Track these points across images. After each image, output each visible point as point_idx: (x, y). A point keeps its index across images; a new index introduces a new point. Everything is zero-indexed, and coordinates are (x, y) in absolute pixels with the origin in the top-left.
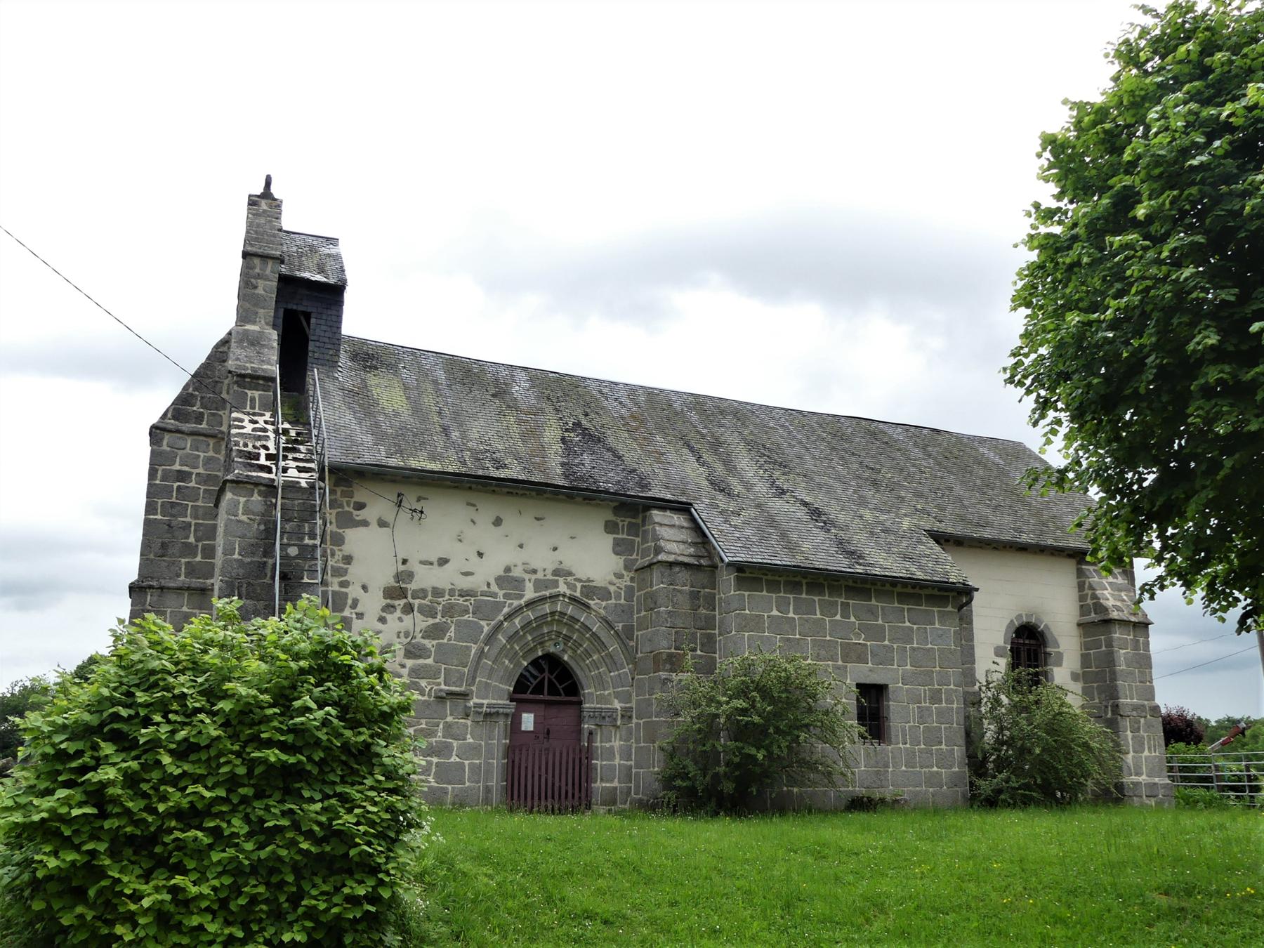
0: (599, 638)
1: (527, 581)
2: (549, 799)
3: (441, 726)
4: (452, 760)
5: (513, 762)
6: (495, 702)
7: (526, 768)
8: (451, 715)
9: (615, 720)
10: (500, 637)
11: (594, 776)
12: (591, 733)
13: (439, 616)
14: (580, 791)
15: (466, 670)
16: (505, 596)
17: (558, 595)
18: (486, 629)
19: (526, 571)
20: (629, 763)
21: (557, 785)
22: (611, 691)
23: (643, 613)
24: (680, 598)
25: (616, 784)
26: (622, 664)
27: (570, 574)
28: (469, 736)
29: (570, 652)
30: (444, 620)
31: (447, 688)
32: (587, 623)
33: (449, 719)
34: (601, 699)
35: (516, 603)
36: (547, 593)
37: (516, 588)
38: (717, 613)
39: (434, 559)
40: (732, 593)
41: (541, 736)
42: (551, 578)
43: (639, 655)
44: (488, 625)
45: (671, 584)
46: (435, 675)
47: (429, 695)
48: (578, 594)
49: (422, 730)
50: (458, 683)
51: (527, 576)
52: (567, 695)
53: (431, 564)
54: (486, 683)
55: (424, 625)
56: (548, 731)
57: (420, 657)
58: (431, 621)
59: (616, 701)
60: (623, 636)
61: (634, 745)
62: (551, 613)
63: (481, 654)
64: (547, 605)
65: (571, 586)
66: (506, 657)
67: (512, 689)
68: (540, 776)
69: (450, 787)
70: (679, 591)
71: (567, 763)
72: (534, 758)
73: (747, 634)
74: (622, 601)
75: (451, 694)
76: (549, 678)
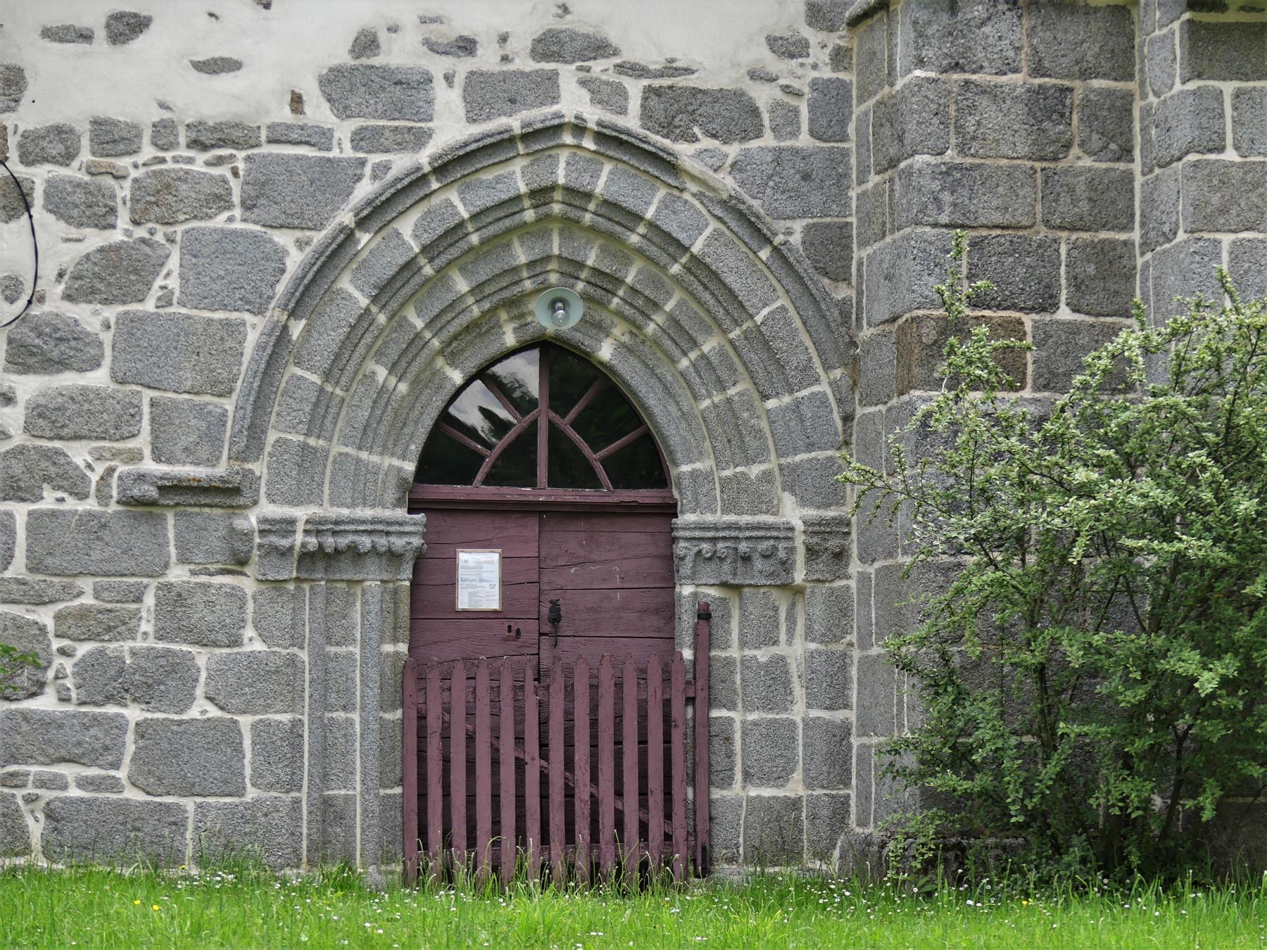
0: (715, 276)
1: (439, 86)
2: (533, 841)
3: (150, 600)
4: (194, 713)
5: (422, 718)
6: (345, 512)
7: (471, 738)
8: (183, 560)
9: (787, 565)
10: (345, 283)
11: (719, 760)
12: (704, 615)
13: (123, 219)
14: (668, 816)
15: (229, 405)
16: (359, 139)
17: (557, 129)
18: (295, 260)
19: (433, 47)
20: (839, 715)
21: (583, 793)
22: (772, 464)
23: (874, 179)
24: (990, 115)
25: (795, 788)
26: (807, 368)
27: (600, 48)
28: (249, 632)
29: (620, 331)
30: (141, 232)
31: (164, 468)
32: (671, 226)
33: (178, 574)
34: (737, 492)
35: (401, 163)
36: (515, 123)
37: (398, 110)
38: (1137, 167)
39: (95, 20)
40: (1178, 86)
41: (529, 629)
42: (530, 65)
43: (866, 333)
44: (301, 245)
45: (957, 67)
46: (123, 425)
47: (103, 497)
48: (631, 121)
49: (83, 614)
50: (204, 452)
51: (438, 66)
52: (617, 483)
53: (85, 36)
54: (304, 447)
55: (69, 255)
56: (555, 605)
57: (62, 365)
58: (94, 239)
59: (788, 500)
60: (805, 267)
61: (856, 654)
62: (533, 194)
63: (279, 340)
64: (517, 167)
65: (609, 96)
66: (379, 356)
67: (410, 467)
68: (520, 765)
69: (189, 804)
70: (984, 91)
71: (618, 718)
72: (495, 703)
73: (1226, 239)
74: (804, 140)
75: (175, 489)
76: (553, 428)
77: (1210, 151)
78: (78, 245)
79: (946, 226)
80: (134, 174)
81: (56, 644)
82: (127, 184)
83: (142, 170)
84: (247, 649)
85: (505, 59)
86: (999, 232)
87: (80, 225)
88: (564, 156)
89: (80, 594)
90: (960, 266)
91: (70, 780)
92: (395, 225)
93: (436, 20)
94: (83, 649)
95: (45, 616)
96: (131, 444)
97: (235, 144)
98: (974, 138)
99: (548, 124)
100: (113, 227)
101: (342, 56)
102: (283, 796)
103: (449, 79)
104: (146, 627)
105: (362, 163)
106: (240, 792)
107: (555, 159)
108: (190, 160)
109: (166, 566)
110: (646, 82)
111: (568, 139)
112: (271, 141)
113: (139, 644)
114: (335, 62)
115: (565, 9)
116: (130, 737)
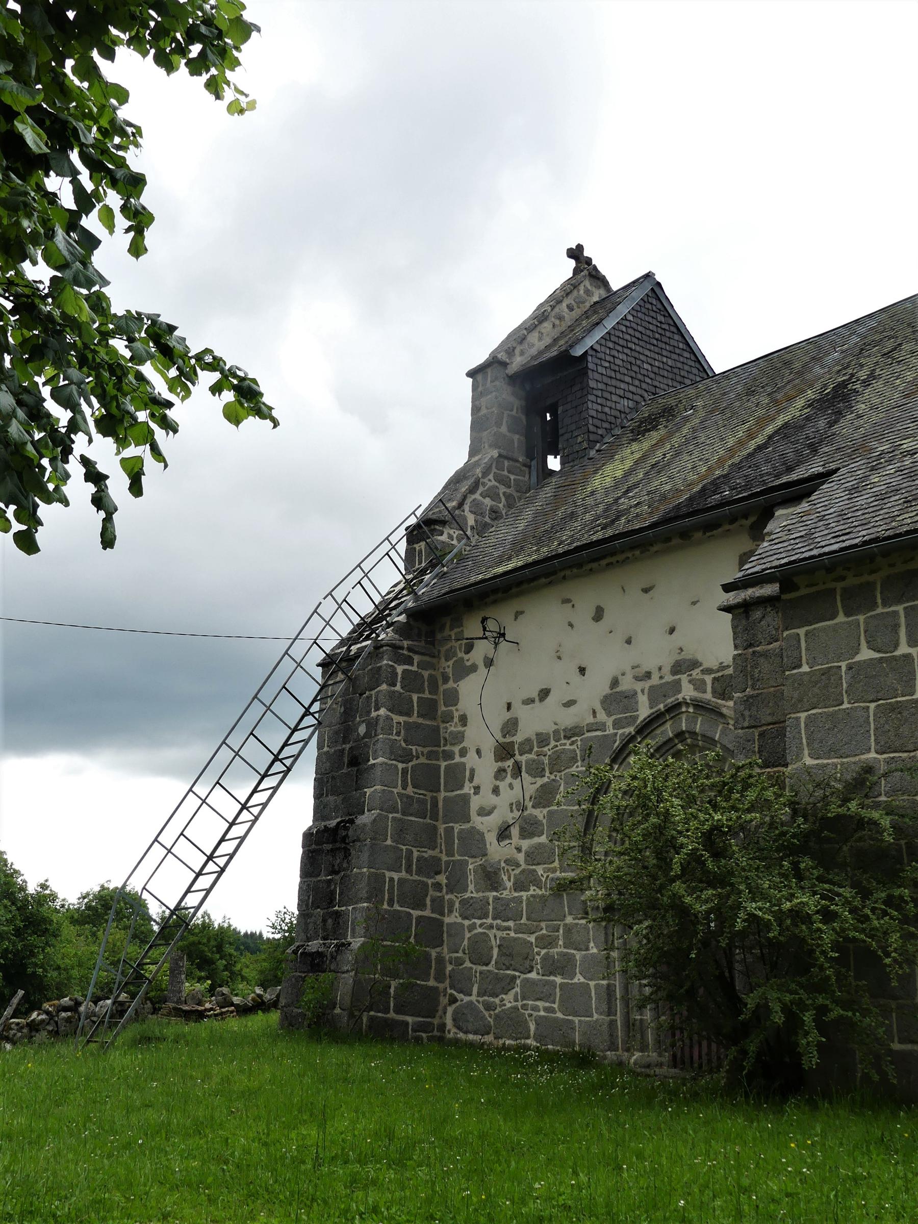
4: (576, 980)
8: (570, 914)
19: (637, 679)
27: (695, 664)
28: (592, 944)
30: (553, 777)
39: (535, 694)
45: (751, 645)
48: (708, 696)
51: (638, 686)
53: (533, 701)
58: (540, 782)
64: (668, 725)
69: (576, 1020)
73: (803, 715)
77: (794, 668)
78: (535, 785)
79: (747, 728)
80: (549, 753)
81: (536, 950)
82: (547, 757)
83: (552, 751)
84: (591, 952)
85: (661, 678)
86: (772, 726)
87: (535, 777)
88: (684, 717)
89: (542, 929)
90: (755, 747)
91: (541, 1007)
92: (627, 760)
93: (638, 666)
94: (543, 952)
95: (532, 939)
96: (552, 866)
97: (578, 735)
98: (758, 680)
99: (673, 704)
100: (544, 776)
101: (607, 691)
102: (606, 1018)
103: (643, 691)
104: (561, 943)
105: (616, 734)
106: (591, 1016)
107: (681, 719)
108: (565, 744)
109: (565, 916)
110: (713, 676)
111: (684, 709)
112: (588, 731)
113: (559, 950)
114: (604, 693)
115: (681, 649)
116: (558, 990)
